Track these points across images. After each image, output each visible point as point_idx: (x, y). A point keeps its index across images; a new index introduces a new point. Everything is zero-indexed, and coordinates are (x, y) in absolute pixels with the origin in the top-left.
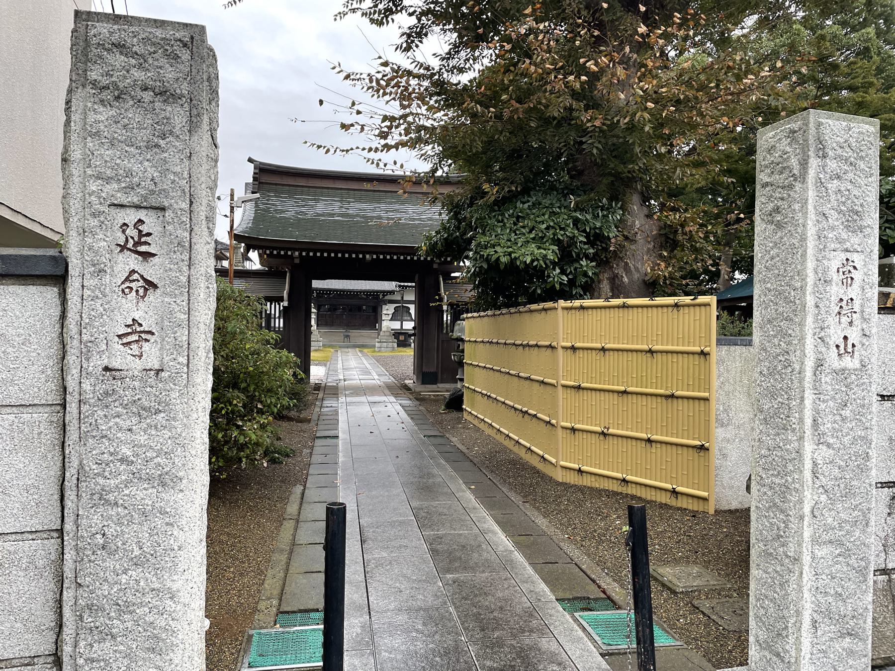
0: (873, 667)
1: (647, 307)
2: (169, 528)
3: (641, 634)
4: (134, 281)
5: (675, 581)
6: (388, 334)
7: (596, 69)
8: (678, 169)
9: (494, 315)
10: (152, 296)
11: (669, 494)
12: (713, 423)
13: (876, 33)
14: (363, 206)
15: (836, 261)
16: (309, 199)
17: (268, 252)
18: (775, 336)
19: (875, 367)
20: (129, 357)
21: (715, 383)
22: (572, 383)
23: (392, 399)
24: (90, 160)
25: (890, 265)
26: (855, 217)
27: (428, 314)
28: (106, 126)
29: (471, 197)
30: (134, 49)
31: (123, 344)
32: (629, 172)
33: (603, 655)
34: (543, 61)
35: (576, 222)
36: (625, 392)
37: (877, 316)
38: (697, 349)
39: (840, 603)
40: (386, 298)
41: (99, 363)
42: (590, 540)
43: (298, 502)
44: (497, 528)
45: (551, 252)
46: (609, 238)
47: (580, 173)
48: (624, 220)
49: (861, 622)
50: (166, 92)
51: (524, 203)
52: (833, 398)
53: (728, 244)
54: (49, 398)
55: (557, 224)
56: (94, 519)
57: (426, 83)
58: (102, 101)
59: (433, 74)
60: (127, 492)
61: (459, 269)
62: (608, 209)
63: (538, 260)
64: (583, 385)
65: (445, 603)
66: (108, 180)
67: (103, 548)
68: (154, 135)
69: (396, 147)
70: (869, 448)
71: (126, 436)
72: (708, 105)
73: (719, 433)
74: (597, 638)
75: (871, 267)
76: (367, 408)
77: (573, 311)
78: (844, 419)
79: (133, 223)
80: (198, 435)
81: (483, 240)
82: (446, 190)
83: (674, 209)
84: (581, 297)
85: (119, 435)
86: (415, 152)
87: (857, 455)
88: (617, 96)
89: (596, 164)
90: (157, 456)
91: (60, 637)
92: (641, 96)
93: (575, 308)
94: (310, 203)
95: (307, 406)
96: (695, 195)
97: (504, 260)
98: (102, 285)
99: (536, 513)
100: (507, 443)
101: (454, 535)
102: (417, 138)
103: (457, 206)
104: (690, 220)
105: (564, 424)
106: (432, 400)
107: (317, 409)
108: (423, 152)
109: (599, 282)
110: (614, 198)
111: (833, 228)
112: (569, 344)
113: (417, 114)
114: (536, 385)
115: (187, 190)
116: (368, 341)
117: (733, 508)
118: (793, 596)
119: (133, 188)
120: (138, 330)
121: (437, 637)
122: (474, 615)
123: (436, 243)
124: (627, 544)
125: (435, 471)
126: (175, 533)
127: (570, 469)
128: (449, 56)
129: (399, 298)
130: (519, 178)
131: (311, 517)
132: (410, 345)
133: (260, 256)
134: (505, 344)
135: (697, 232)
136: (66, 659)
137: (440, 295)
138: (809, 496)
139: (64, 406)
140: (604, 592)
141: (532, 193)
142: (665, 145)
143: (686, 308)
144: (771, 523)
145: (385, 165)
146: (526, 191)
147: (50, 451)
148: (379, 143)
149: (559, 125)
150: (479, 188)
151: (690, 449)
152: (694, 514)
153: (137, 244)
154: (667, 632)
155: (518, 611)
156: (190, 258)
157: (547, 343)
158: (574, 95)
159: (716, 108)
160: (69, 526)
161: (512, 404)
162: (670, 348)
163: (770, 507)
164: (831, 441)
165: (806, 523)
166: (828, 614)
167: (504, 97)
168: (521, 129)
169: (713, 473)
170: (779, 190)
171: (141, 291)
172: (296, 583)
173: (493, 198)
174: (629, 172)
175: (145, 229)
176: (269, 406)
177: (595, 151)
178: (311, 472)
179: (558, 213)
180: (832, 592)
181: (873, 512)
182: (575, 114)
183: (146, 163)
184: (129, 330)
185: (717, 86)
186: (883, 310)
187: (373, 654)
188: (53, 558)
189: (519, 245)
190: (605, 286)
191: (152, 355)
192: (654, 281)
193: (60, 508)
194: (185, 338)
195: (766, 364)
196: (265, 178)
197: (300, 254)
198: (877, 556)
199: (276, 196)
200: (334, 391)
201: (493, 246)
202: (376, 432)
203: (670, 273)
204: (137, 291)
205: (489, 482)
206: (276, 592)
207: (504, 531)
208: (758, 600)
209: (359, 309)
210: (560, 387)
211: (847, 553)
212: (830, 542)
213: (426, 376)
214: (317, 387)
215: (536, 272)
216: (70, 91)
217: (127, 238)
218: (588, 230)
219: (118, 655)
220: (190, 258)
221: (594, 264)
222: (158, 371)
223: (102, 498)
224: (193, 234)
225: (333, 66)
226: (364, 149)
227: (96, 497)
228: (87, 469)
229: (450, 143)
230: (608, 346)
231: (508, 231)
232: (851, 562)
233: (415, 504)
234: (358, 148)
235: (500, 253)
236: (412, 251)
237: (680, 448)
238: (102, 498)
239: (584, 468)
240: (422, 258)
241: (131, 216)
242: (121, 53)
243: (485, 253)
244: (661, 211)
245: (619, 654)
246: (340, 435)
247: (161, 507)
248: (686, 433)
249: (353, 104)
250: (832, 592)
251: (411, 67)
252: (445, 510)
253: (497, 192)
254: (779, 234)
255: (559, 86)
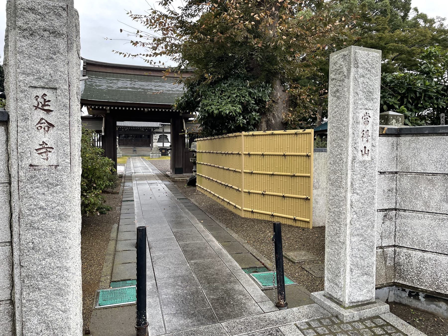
0: (376, 289)
1: (283, 134)
2: (64, 239)
3: (279, 279)
4: (43, 123)
5: (294, 258)
6: (156, 149)
7: (259, 19)
8: (298, 68)
9: (211, 139)
10: (52, 131)
11: (292, 221)
12: (312, 188)
13: (390, 3)
14: (143, 83)
15: (361, 114)
16: (114, 80)
17: (93, 107)
18: (336, 147)
19: (377, 160)
20: (42, 160)
21: (313, 169)
22: (248, 171)
23: (160, 181)
24: (19, 65)
25: (388, 115)
26: (370, 94)
27: (177, 138)
28: (26, 49)
29: (199, 81)
30: (39, 11)
31: (38, 154)
32: (275, 69)
33: (262, 290)
34: (233, 14)
35: (250, 93)
36: (273, 175)
37: (379, 138)
38: (305, 154)
39: (362, 261)
40: (155, 131)
41: (27, 162)
42: (257, 243)
43: (116, 232)
44: (214, 239)
45: (238, 108)
46: (265, 102)
47: (252, 69)
48: (272, 93)
49: (371, 269)
50: (55, 32)
51: (225, 84)
52: (360, 173)
53: (320, 105)
54: (2, 180)
55: (241, 94)
56: (28, 236)
57: (174, 22)
58: (24, 36)
59: (178, 17)
60: (43, 223)
61: (193, 116)
62: (265, 87)
63: (232, 112)
64: (254, 172)
65: (191, 273)
66: (28, 75)
67: (33, 249)
68: (50, 53)
69: (160, 54)
70: (374, 194)
71: (42, 197)
72: (311, 38)
73: (315, 192)
74: (260, 283)
75: (376, 116)
76: (147, 186)
77: (249, 137)
78: (364, 182)
79: (41, 95)
80: (76, 196)
81: (205, 102)
82: (186, 76)
83: (296, 88)
84: (253, 130)
85: (38, 196)
86: (170, 57)
87: (369, 197)
88: (269, 32)
89: (259, 65)
90: (57, 206)
91: (13, 291)
92: (280, 33)
93: (250, 136)
94: (114, 81)
95: (116, 186)
96: (306, 80)
97: (216, 112)
98: (27, 125)
99: (232, 232)
100: (218, 201)
101: (194, 243)
102: (171, 50)
103: (192, 85)
104: (303, 93)
105: (245, 153)
106: (180, 182)
107: (122, 187)
108: (174, 57)
109: (261, 123)
110: (267, 82)
111: (360, 99)
112: (247, 153)
113: (171, 37)
114: (232, 172)
115: (67, 80)
116: (146, 153)
117: (320, 226)
118: (343, 258)
119: (40, 79)
120: (46, 146)
121: (188, 287)
122: (205, 277)
123: (182, 103)
124: (273, 240)
125: (184, 215)
126: (67, 241)
127: (248, 211)
128: (186, 8)
129: (162, 131)
130: (222, 71)
131: (123, 238)
132: (168, 155)
133: (88, 109)
134: (217, 153)
135: (306, 99)
136: (17, 301)
137: (183, 129)
138: (349, 216)
139: (10, 183)
140: (263, 264)
141: (229, 79)
142: (291, 57)
143: (300, 135)
144: (334, 228)
145: (155, 63)
146: (226, 78)
147: (4, 205)
148: (151, 52)
149: (242, 45)
150: (203, 76)
151: (302, 200)
152: (303, 229)
153: (44, 105)
154: (290, 279)
155: (225, 275)
156: (70, 113)
157: (237, 152)
158: (248, 30)
159: (315, 39)
160: (15, 239)
161: (220, 182)
162: (293, 153)
163: (333, 221)
164: (358, 192)
165: (348, 227)
166: (357, 266)
167: (214, 31)
168: (223, 47)
169: (312, 210)
170: (339, 82)
171: (46, 128)
172: (119, 268)
173: (210, 81)
174: (275, 69)
175: (47, 98)
176: (99, 185)
177: (259, 59)
178: (121, 217)
179: (241, 89)
180: (359, 256)
181: (376, 222)
182: (249, 40)
183: (47, 67)
184: (41, 147)
185: (315, 28)
186: (380, 135)
187: (158, 296)
188: (8, 255)
189: (223, 105)
190: (264, 125)
191: (53, 158)
192: (286, 122)
193: (10, 232)
194: (69, 150)
195: (332, 159)
196: (89, 68)
197: (110, 108)
198: (378, 241)
199: (96, 78)
200: (130, 178)
201: (211, 105)
202: (153, 198)
203: (294, 118)
204: (44, 128)
205: (210, 219)
206: (109, 273)
207: (217, 240)
208: (328, 261)
209: (141, 136)
210: (243, 173)
211: (364, 240)
212: (358, 235)
213: (177, 170)
214: (121, 177)
215: (231, 118)
216: (7, 31)
217: (38, 103)
218: (256, 98)
219: (42, 298)
220: (70, 113)
221: (258, 114)
222: (56, 166)
223: (31, 226)
224: (71, 101)
225: (127, 12)
226: (144, 55)
227: (28, 225)
228: (24, 212)
229: (187, 53)
230: (265, 153)
231: (217, 97)
232: (366, 243)
233: (175, 230)
234: (140, 54)
235: (214, 109)
236: (170, 107)
237: (297, 199)
238: (31, 226)
239: (254, 210)
240: (174, 111)
241: (40, 92)
242: (33, 13)
243: (206, 109)
244: (290, 88)
245: (270, 289)
246: (135, 200)
247: (60, 229)
248: (300, 192)
249: (138, 32)
250: (359, 256)
251: (167, 13)
252: (189, 233)
253: (212, 78)
254: (338, 102)
255: (242, 26)
